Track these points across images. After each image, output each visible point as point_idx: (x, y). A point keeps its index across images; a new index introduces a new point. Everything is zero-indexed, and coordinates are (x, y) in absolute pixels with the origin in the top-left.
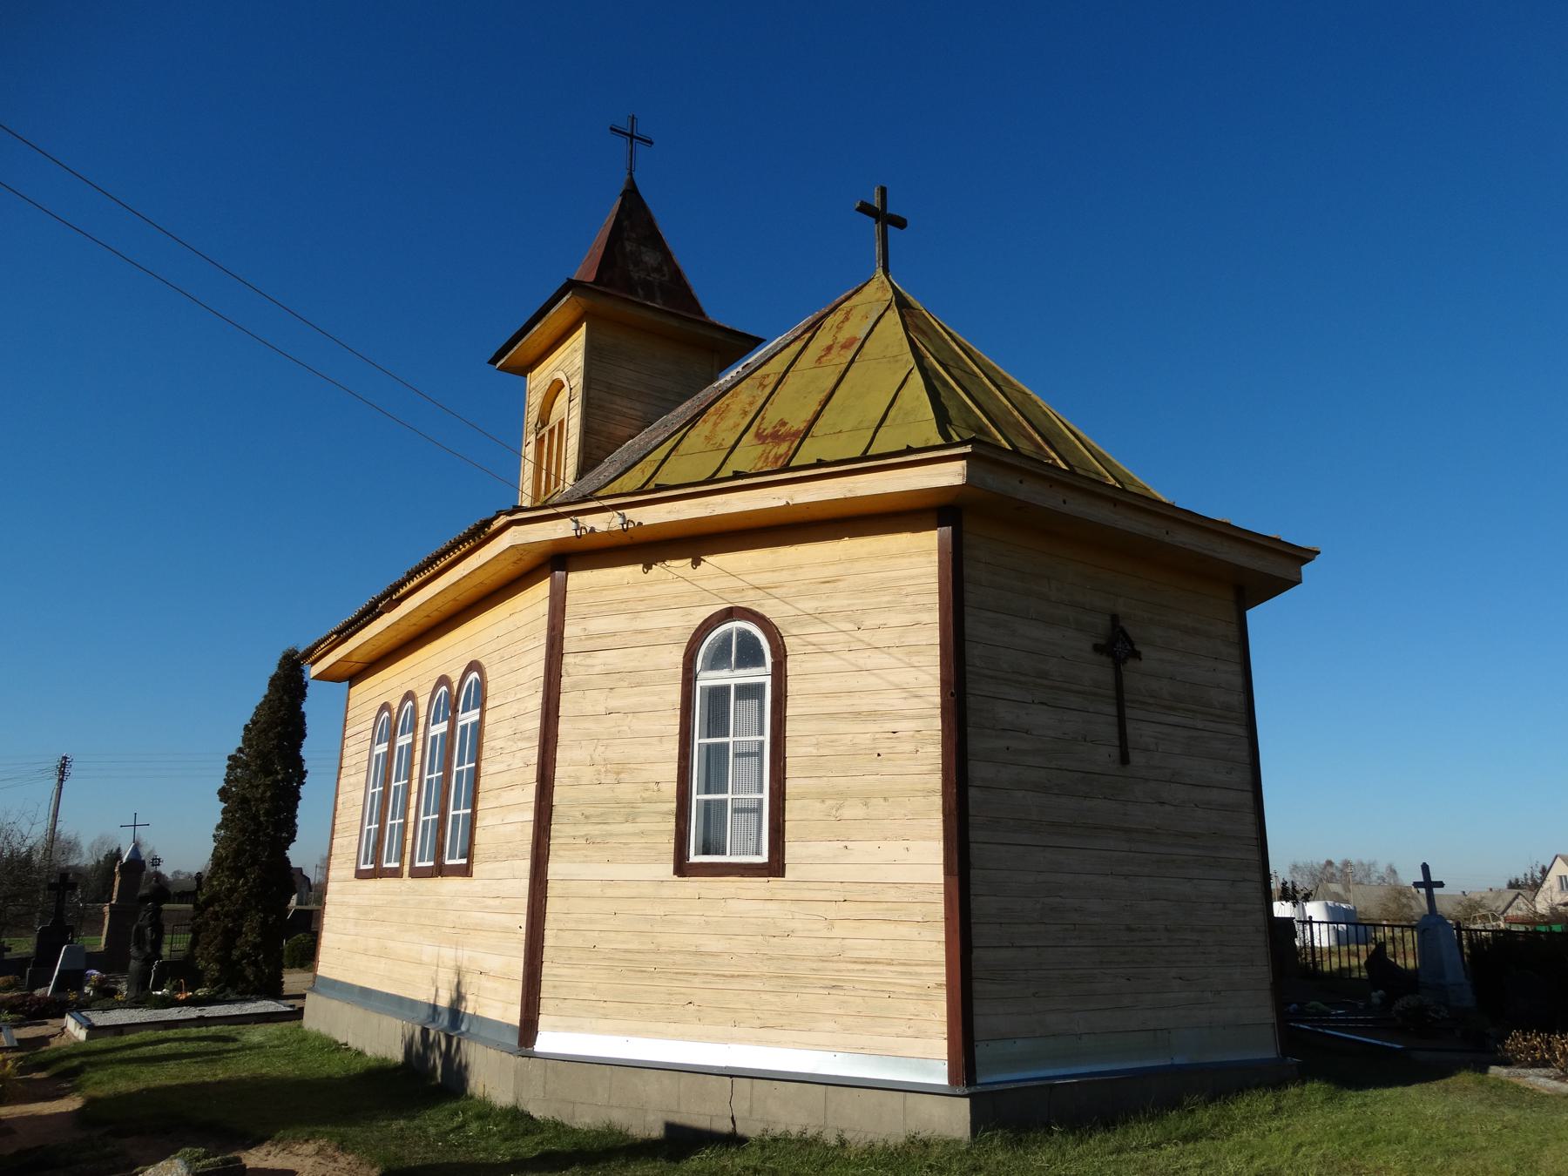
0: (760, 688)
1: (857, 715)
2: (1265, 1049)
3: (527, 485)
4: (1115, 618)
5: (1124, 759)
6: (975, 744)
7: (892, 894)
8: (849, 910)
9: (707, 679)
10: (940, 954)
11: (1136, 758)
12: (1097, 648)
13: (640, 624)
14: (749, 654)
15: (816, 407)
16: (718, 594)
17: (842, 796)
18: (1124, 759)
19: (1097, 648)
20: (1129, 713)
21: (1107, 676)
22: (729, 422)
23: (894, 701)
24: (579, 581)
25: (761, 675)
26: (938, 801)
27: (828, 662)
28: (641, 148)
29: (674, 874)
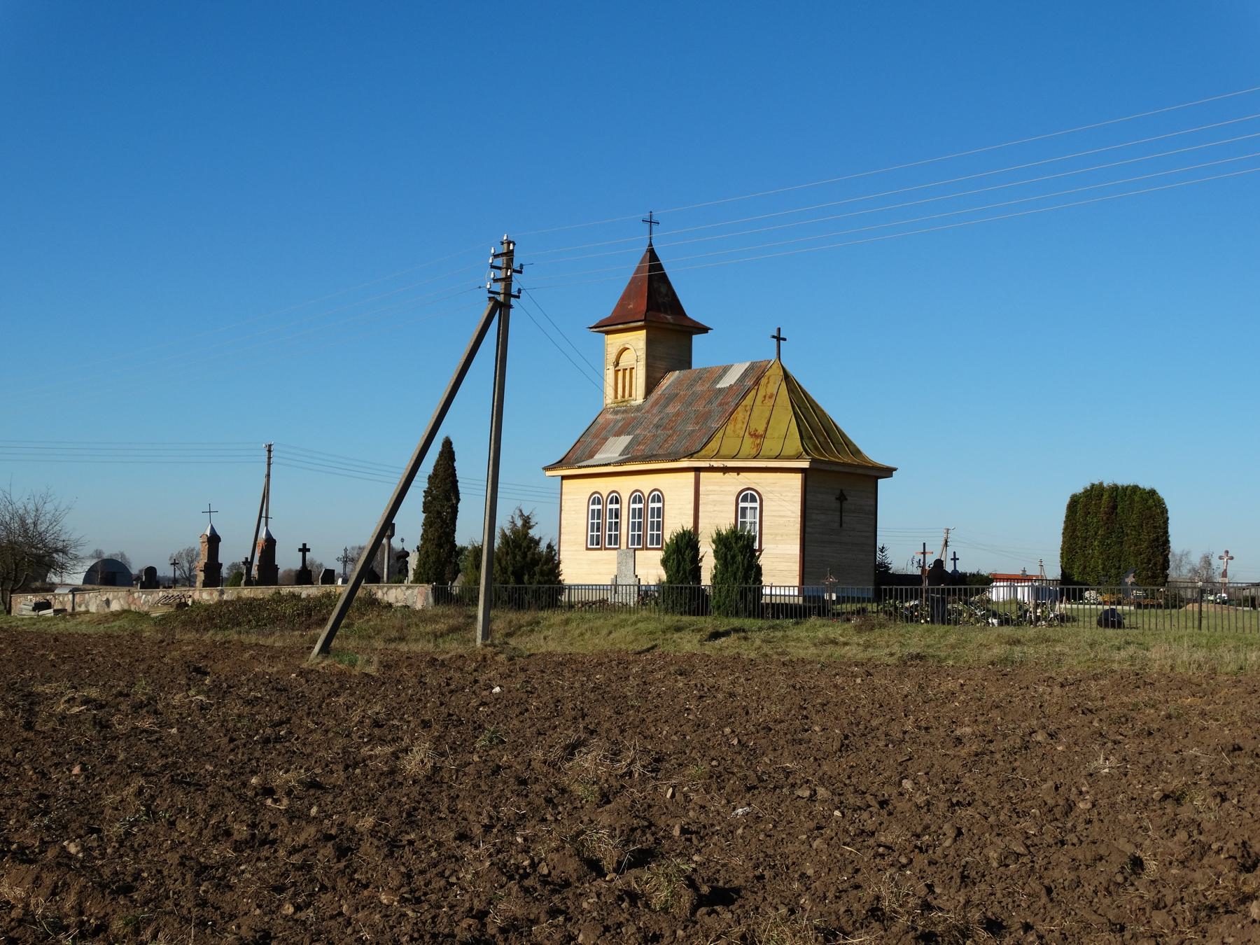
0: (756, 508)
1: (780, 516)
2: (871, 595)
3: (609, 391)
4: (841, 491)
5: (841, 526)
6: (807, 524)
7: (787, 556)
8: (778, 560)
9: (742, 505)
10: (798, 569)
11: (844, 525)
12: (837, 499)
13: (722, 489)
14: (753, 499)
15: (765, 426)
16: (744, 484)
17: (776, 535)
18: (841, 526)
19: (837, 499)
20: (843, 514)
21: (838, 505)
22: (739, 426)
23: (789, 513)
24: (702, 474)
25: (757, 505)
26: (799, 536)
27: (774, 503)
28: (654, 226)
29: (326, 570)
